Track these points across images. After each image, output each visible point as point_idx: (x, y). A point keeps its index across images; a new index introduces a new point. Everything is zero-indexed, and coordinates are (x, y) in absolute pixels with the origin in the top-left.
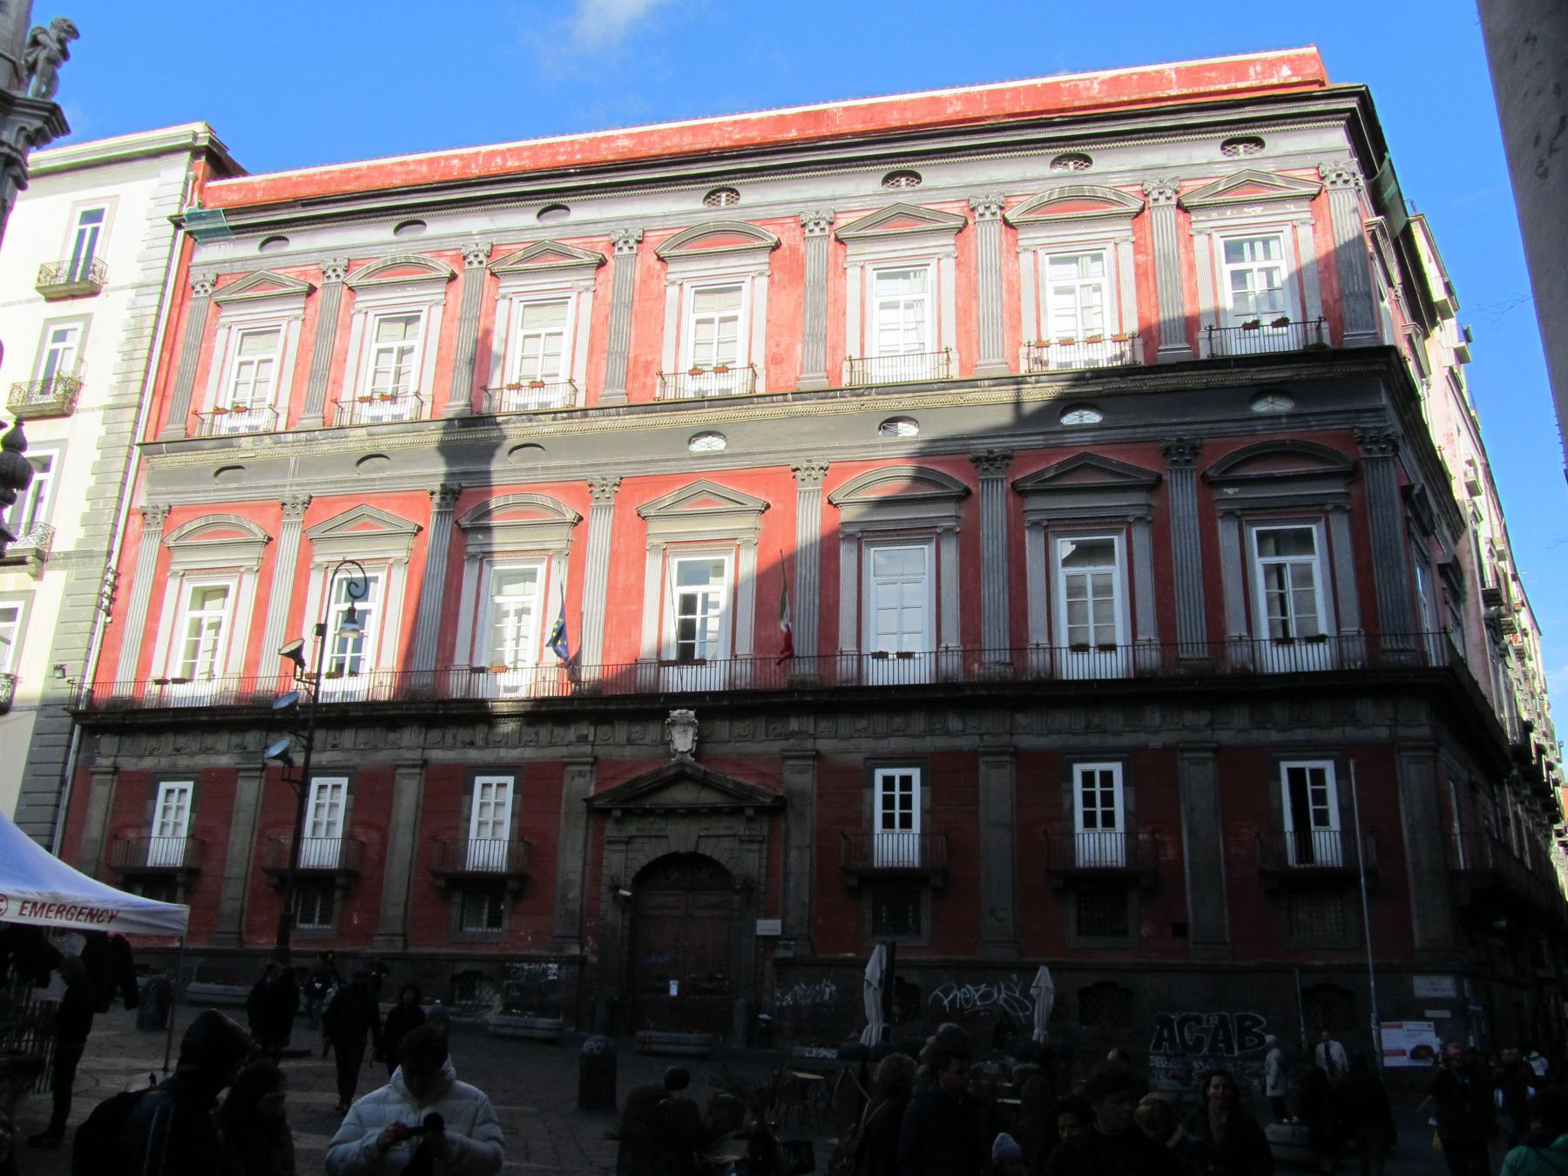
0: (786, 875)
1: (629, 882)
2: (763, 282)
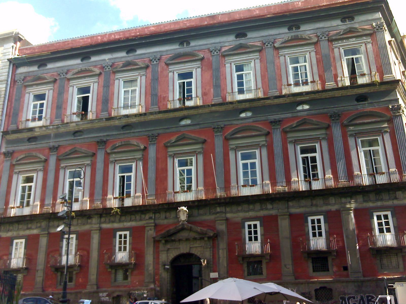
1: (169, 263)
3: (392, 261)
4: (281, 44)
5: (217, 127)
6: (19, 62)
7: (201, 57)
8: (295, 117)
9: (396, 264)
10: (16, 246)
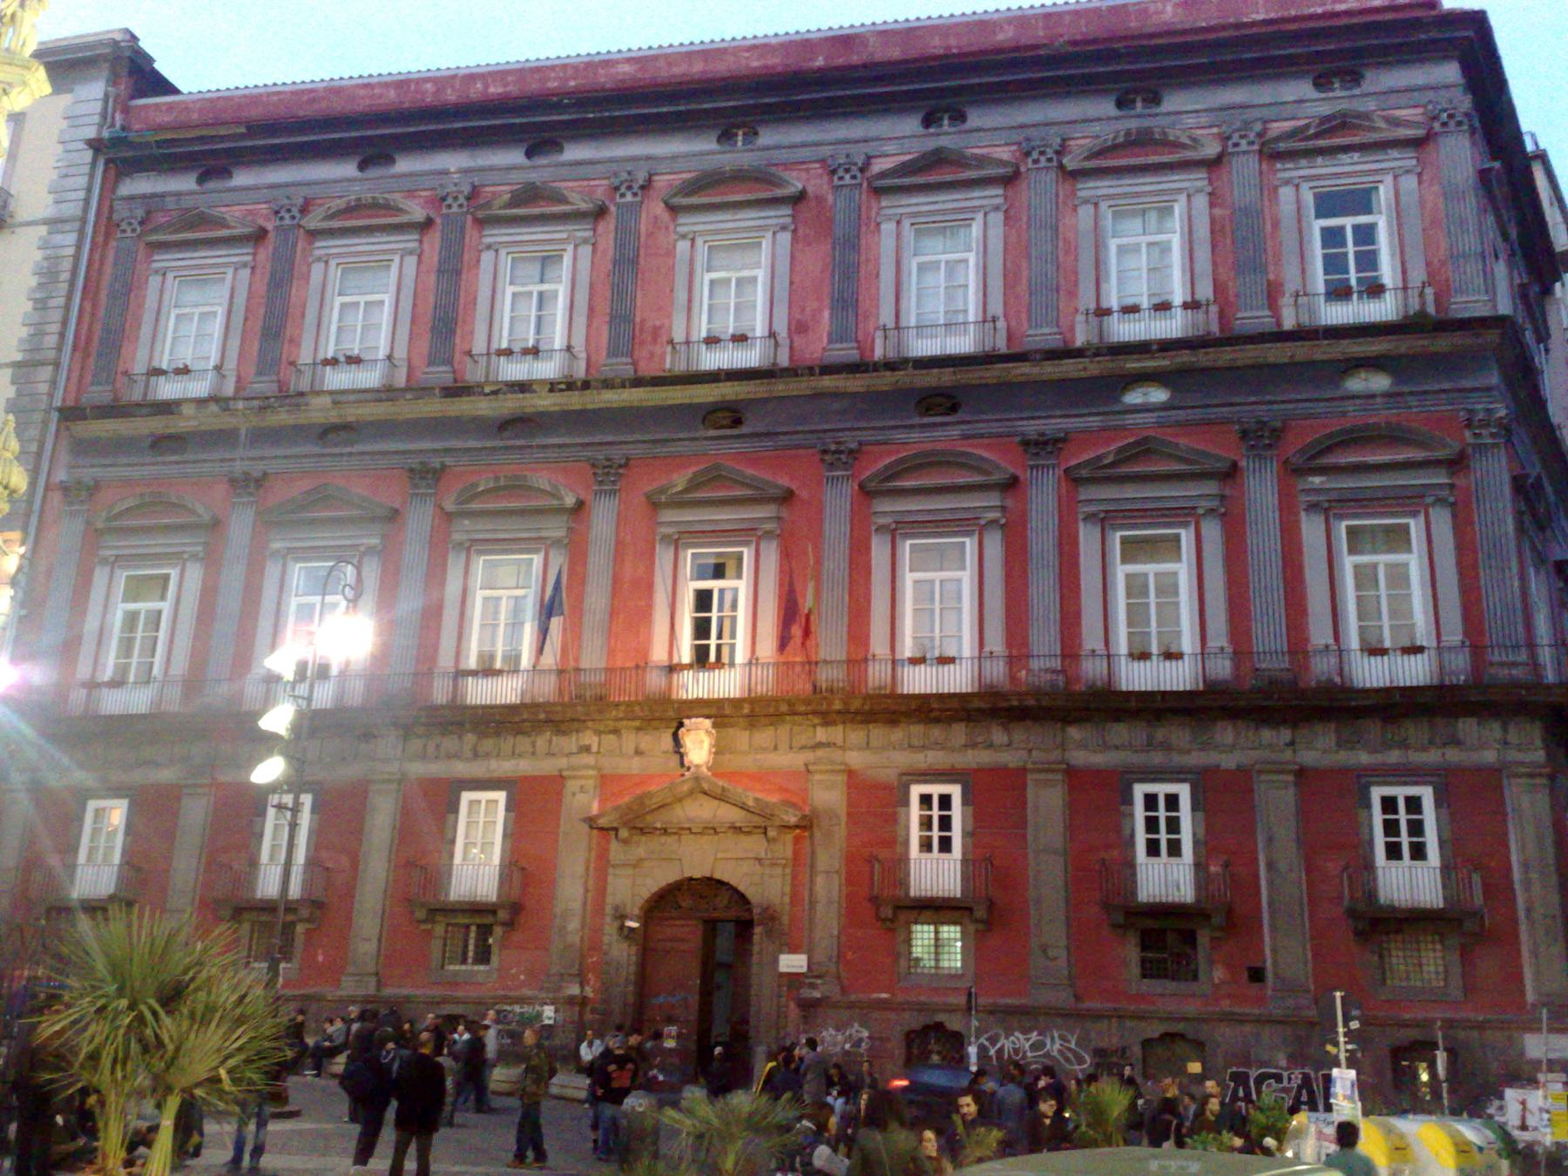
0: (813, 903)
1: (636, 911)
2: (785, 238)
3: (1424, 961)
4: (1087, 158)
5: (833, 447)
6: (131, 154)
7: (793, 190)
8: (1116, 428)
9: (1437, 973)
10: (95, 822)
